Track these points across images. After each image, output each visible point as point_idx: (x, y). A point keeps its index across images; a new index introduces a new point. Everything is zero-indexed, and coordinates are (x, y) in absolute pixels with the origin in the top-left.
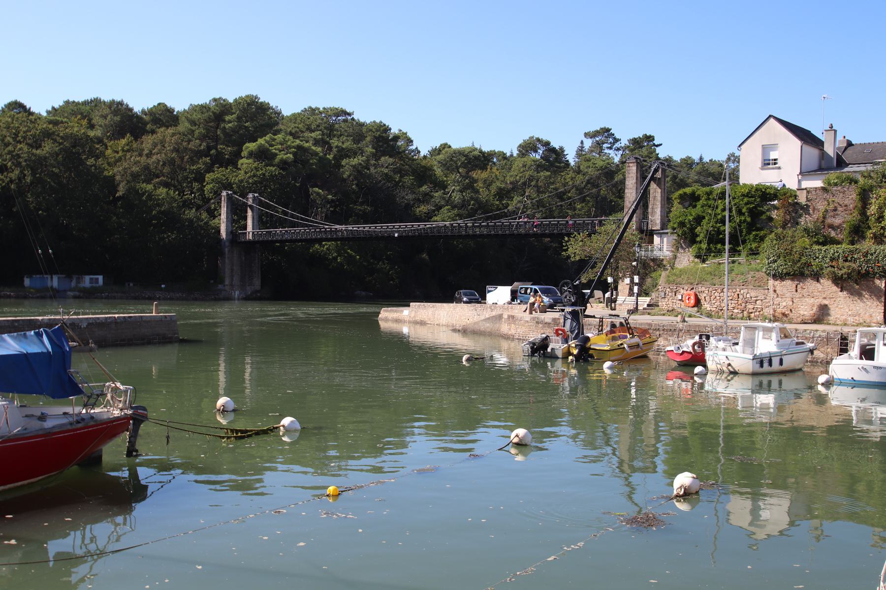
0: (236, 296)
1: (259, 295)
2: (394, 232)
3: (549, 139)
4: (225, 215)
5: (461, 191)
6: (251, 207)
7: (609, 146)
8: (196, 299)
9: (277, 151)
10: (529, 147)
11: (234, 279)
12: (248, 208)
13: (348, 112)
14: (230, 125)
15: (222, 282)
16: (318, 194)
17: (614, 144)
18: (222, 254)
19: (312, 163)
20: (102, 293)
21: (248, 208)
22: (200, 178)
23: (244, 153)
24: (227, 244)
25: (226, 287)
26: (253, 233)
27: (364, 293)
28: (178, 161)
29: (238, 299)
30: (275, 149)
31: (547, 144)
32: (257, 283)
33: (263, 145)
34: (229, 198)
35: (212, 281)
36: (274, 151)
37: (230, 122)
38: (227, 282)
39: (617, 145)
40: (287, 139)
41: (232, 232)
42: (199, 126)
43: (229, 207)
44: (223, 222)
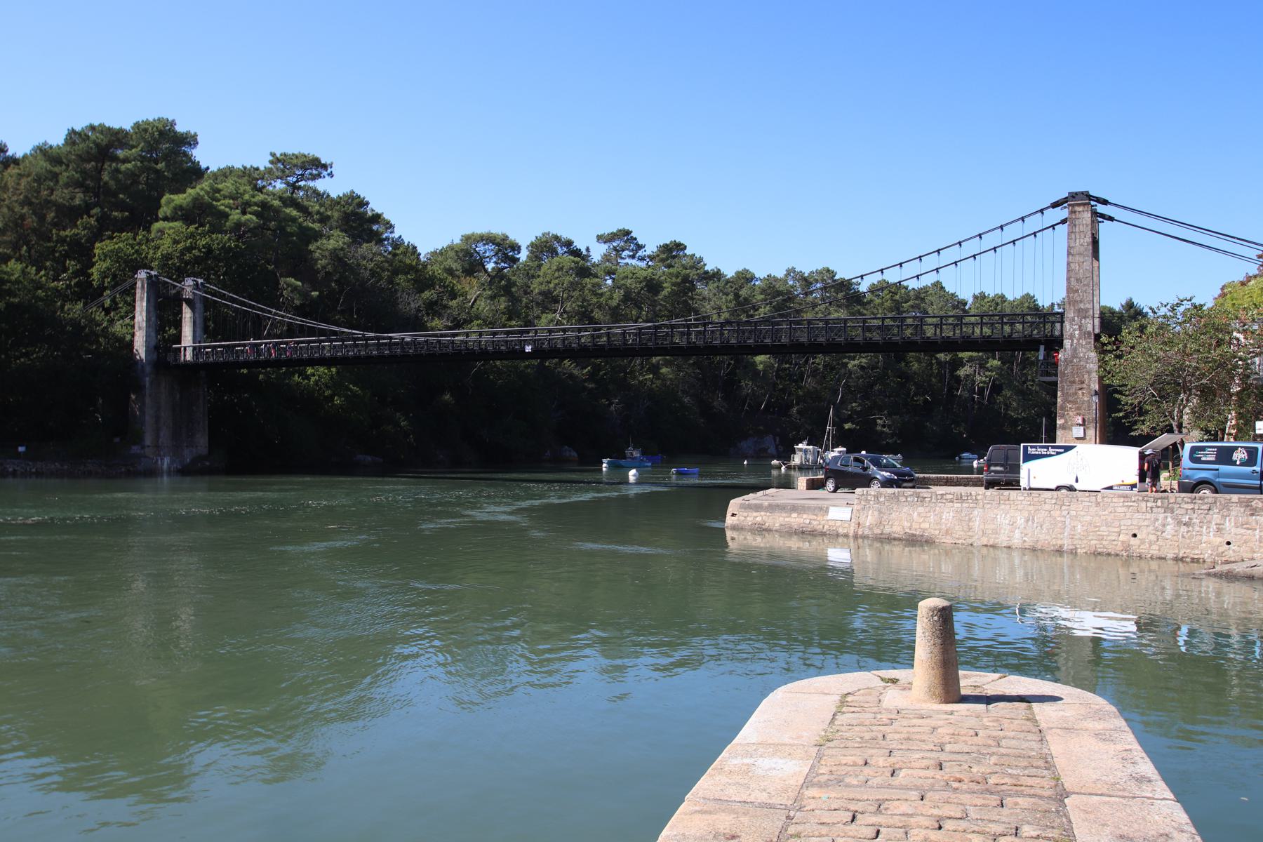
0: (165, 466)
1: (208, 464)
2: (523, 343)
3: (572, 238)
4: (144, 314)
5: (492, 298)
6: (190, 303)
7: (631, 253)
8: (89, 474)
9: (227, 210)
10: (545, 246)
11: (162, 434)
12: (184, 305)
13: (323, 162)
14: (129, 166)
15: (139, 440)
16: (295, 289)
17: (637, 251)
18: (139, 389)
19: (291, 233)
20: (250, 513)
21: (184, 305)
22: (83, 252)
23: (164, 210)
24: (148, 369)
25: (147, 450)
26: (194, 348)
27: (369, 458)
28: (31, 221)
29: (169, 473)
30: (223, 205)
31: (569, 243)
32: (202, 441)
33: (202, 197)
34: (153, 283)
35: (117, 440)
36: (223, 207)
37: (126, 161)
38: (148, 441)
39: (640, 253)
40: (241, 191)
41: (157, 348)
42: (68, 166)
43: (152, 300)
44: (140, 328)
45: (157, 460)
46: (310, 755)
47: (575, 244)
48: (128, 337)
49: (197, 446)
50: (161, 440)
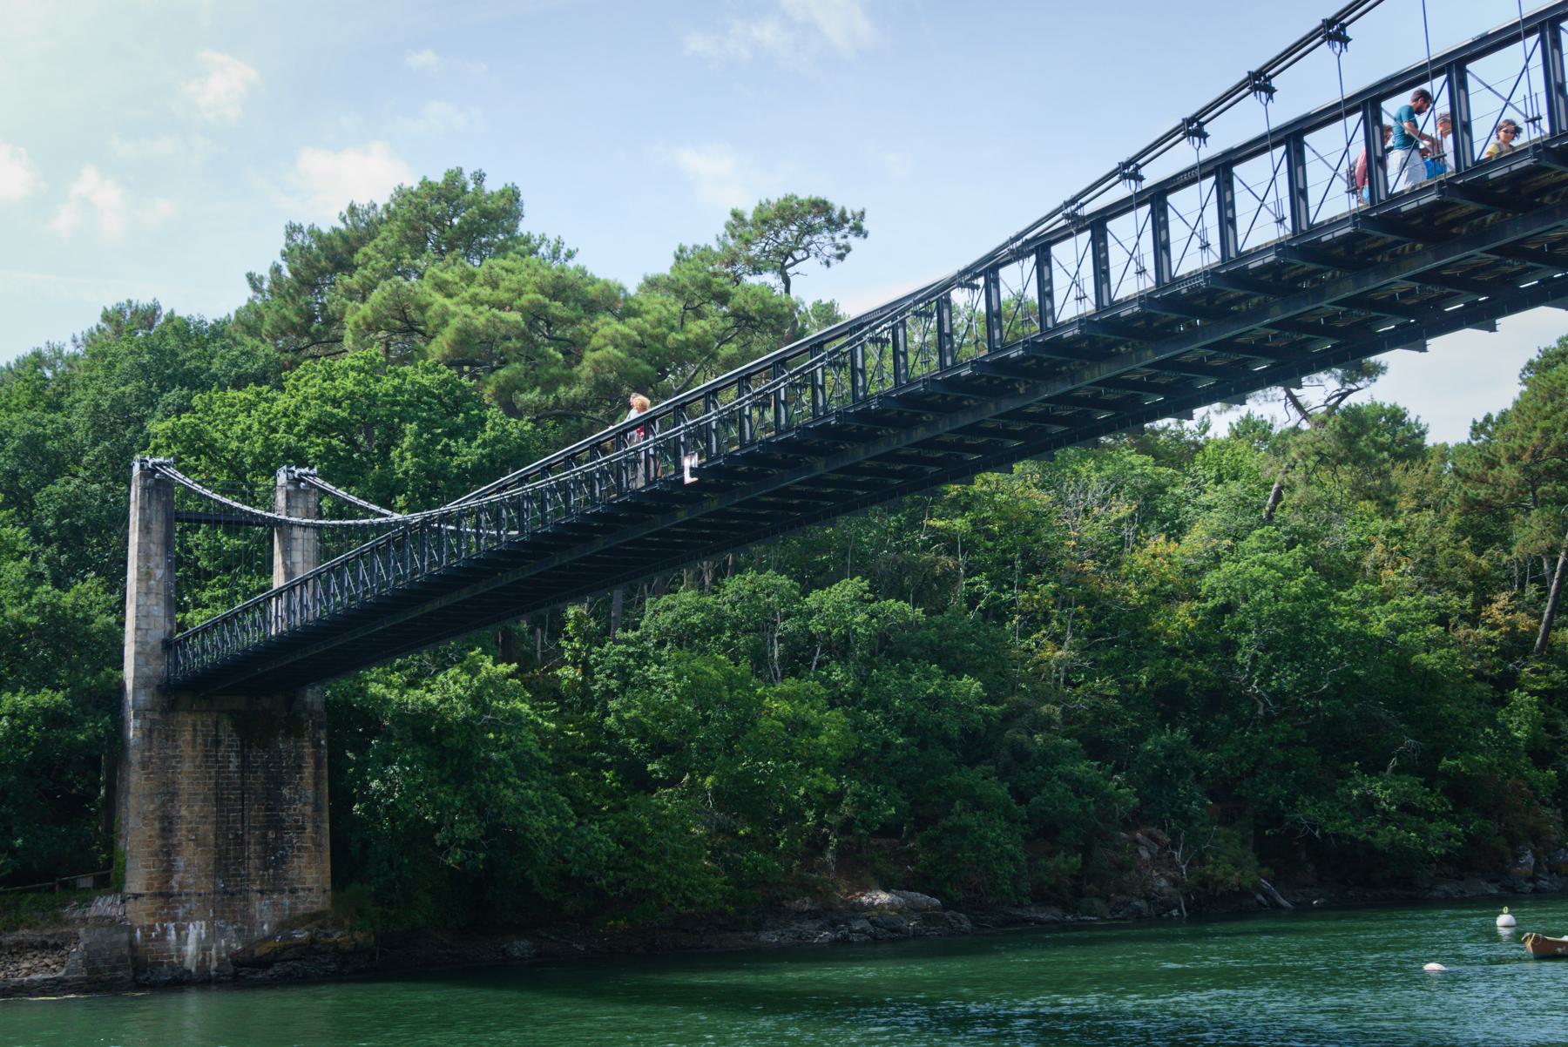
11: (181, 863)
45: (165, 931)
46: (1118, 497)
47: (165, 311)
48: (104, 620)
49: (293, 891)
50: (177, 877)
